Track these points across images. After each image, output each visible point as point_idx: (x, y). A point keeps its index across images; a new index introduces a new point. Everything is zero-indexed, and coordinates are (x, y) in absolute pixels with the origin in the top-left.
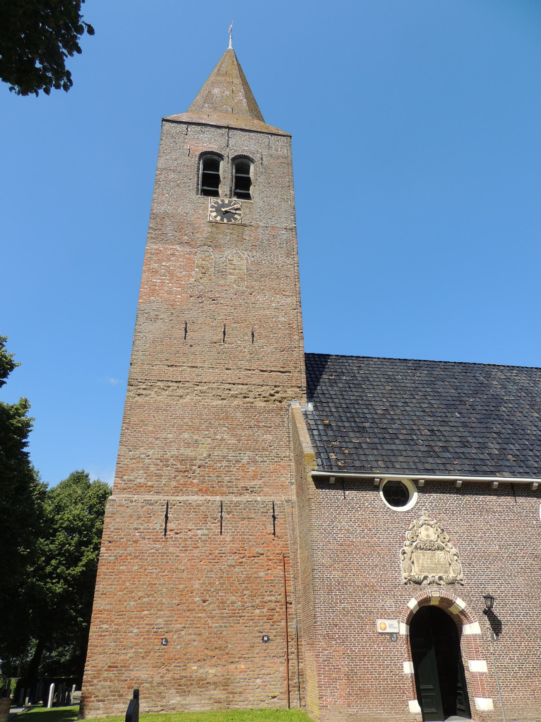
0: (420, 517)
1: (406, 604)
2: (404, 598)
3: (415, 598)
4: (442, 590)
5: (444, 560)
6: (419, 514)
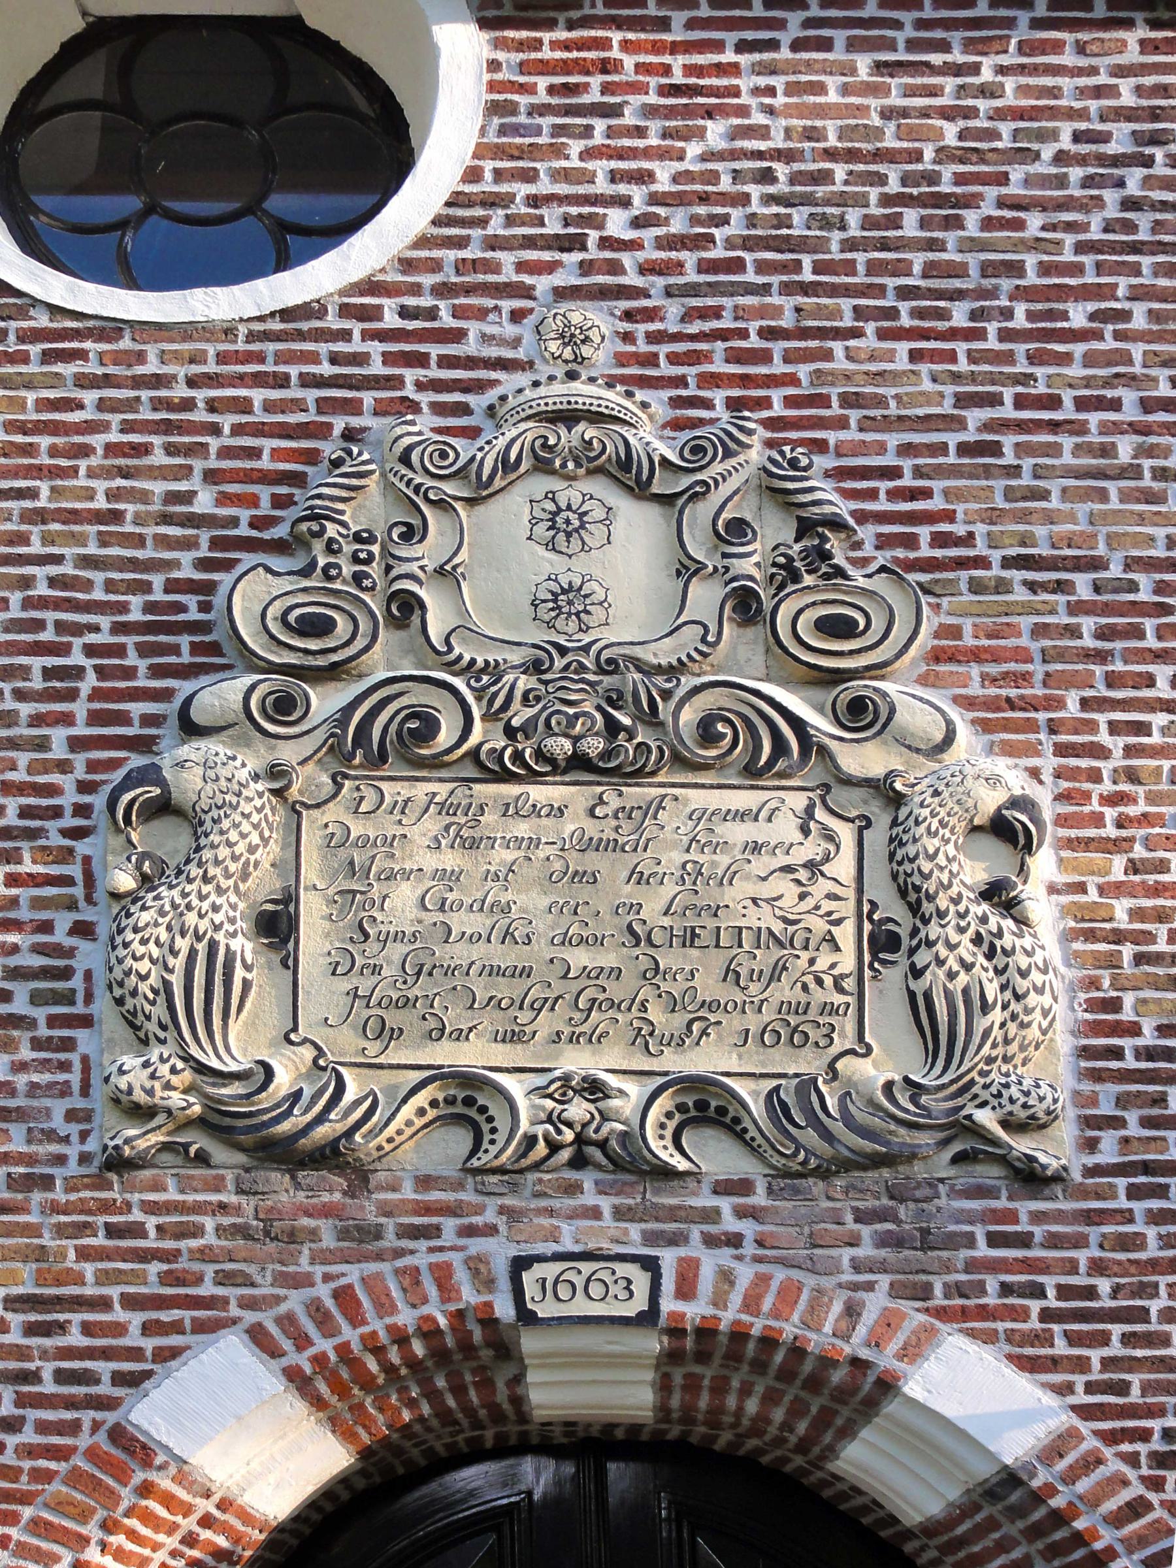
0: (479, 386)
1: (107, 1404)
2: (75, 1338)
3: (258, 1336)
4: (695, 1248)
5: (784, 887)
6: (471, 347)
